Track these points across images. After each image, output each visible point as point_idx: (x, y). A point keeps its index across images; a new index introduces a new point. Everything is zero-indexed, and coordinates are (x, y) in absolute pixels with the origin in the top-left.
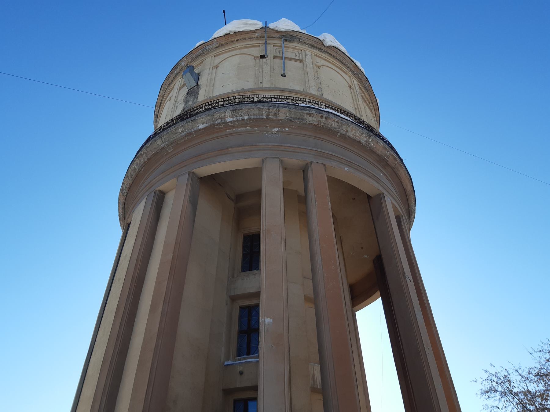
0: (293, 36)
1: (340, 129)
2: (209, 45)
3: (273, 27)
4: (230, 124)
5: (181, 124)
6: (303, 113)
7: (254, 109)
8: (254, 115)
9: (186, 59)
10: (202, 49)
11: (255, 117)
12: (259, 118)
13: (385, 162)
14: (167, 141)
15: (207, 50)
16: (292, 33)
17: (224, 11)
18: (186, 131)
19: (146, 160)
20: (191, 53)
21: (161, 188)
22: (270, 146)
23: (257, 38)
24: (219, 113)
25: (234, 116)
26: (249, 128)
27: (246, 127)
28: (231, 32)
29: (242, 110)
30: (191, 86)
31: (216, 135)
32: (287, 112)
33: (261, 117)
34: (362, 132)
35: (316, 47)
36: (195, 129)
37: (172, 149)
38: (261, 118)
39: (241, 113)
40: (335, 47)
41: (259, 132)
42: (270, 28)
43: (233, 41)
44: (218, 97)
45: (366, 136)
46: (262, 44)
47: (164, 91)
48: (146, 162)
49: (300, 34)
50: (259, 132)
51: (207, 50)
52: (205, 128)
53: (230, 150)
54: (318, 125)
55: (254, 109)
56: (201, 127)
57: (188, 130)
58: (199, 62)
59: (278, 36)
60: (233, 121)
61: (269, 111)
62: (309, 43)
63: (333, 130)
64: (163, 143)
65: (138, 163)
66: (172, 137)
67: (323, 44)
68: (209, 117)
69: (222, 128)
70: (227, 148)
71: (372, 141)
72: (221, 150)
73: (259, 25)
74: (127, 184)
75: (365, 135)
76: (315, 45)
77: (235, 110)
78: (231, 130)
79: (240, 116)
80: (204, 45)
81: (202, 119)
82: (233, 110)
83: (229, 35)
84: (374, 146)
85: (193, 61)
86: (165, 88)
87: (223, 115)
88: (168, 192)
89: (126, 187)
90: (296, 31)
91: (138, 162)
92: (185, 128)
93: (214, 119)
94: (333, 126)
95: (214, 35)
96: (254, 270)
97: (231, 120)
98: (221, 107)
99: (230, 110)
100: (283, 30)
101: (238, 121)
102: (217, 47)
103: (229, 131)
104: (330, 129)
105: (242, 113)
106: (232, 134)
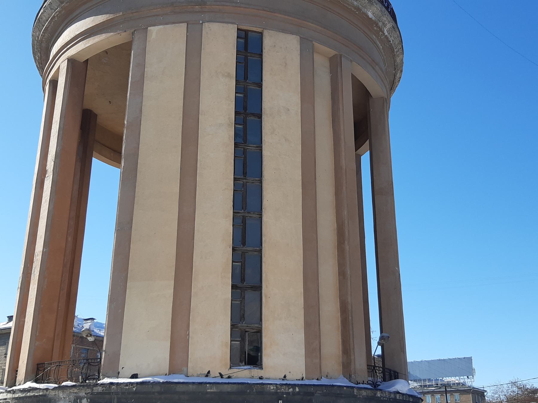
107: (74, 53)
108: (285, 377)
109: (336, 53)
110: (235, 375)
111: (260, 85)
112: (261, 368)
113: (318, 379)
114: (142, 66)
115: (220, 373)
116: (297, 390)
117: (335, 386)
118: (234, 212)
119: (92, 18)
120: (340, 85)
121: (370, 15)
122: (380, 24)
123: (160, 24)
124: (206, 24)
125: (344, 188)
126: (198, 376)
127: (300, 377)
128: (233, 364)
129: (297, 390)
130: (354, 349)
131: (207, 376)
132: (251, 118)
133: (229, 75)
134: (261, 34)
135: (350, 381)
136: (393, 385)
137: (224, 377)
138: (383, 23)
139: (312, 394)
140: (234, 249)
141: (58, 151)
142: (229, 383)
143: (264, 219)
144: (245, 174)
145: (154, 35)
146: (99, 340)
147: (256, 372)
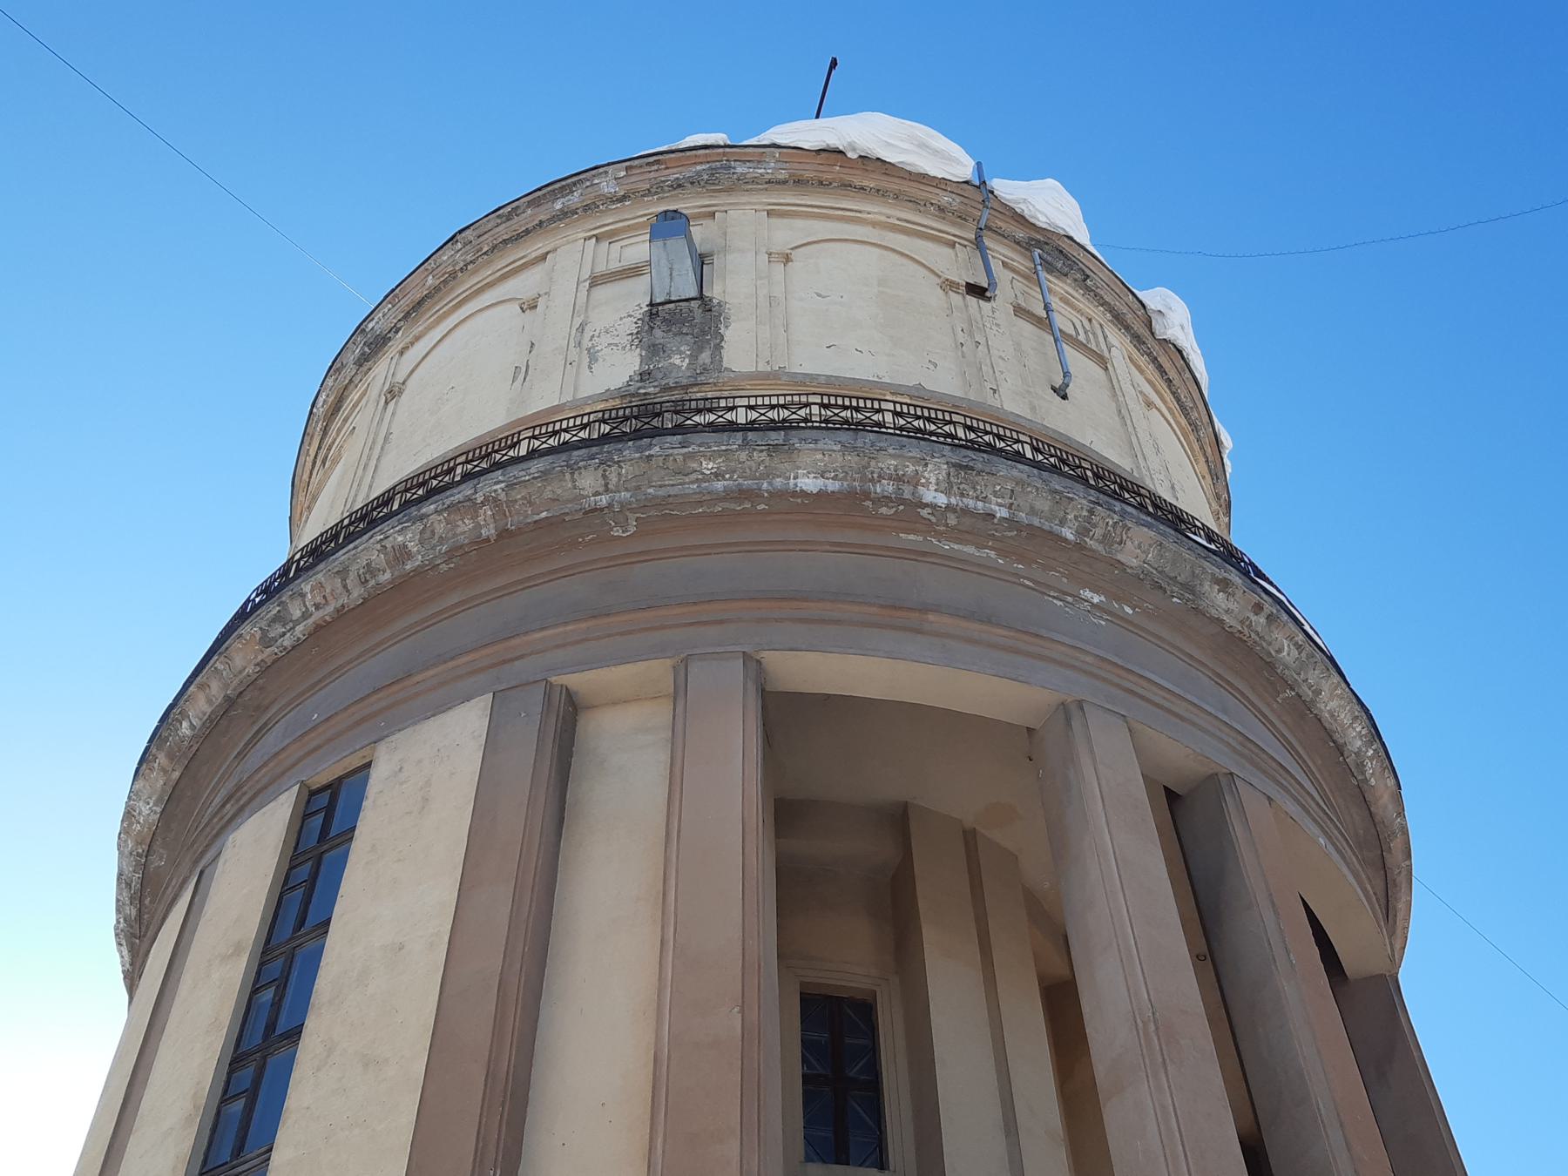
0: (1066, 257)
1: (1299, 674)
2: (745, 162)
3: (1008, 197)
4: (925, 512)
5: (719, 444)
6: (1204, 571)
7: (1037, 489)
8: (1033, 511)
9: (623, 173)
10: (714, 165)
11: (1036, 522)
12: (1050, 532)
13: (1380, 852)
14: (627, 490)
15: (735, 176)
16: (1065, 245)
17: (834, 63)
18: (731, 478)
19: (489, 531)
20: (657, 162)
21: (574, 680)
22: (1089, 659)
23: (941, 209)
24: (899, 456)
25: (955, 488)
26: (993, 554)
27: (980, 546)
28: (854, 150)
29: (992, 479)
30: (669, 294)
31: (853, 536)
32: (1150, 546)
33: (1056, 529)
34: (1356, 713)
35: (1127, 328)
36: (778, 482)
37: (633, 529)
38: (1057, 535)
39: (986, 486)
40: (1180, 352)
41: (1031, 584)
42: (996, 192)
43: (846, 186)
44: (828, 385)
45: (1363, 733)
46: (966, 243)
47: (469, 258)
48: (488, 540)
49: (1089, 260)
50: (1031, 584)
51: (735, 176)
52: (822, 495)
53: (931, 617)
54: (1237, 635)
55: (1037, 489)
56: (809, 484)
57: (746, 478)
58: (696, 211)
59: (1021, 234)
60: (949, 507)
61: (1088, 520)
62: (1112, 303)
63: (1279, 671)
64: (607, 490)
65: (433, 533)
66: (662, 479)
67: (1149, 324)
68: (852, 459)
69: (886, 517)
70: (924, 609)
71: (1371, 759)
72: (894, 607)
73: (961, 166)
74: (319, 599)
75: (1363, 728)
76: (1129, 317)
77: (967, 467)
78: (921, 538)
79: (977, 498)
80: (724, 154)
81: (819, 456)
82: (958, 466)
83: (840, 156)
84: (1372, 780)
85: (656, 193)
86: (482, 249)
87: (912, 468)
88: (588, 708)
89: (306, 615)
90: (1078, 240)
91: (440, 529)
92: (733, 464)
93: (873, 472)
94: (1281, 655)
95: (771, 130)
96: (854, 1165)
97: (942, 500)
98: (895, 434)
99: (947, 463)
100: (1042, 221)
101: (966, 511)
102: (779, 182)
103: (911, 537)
104: (1271, 666)
105: (990, 489)
106: (925, 554)
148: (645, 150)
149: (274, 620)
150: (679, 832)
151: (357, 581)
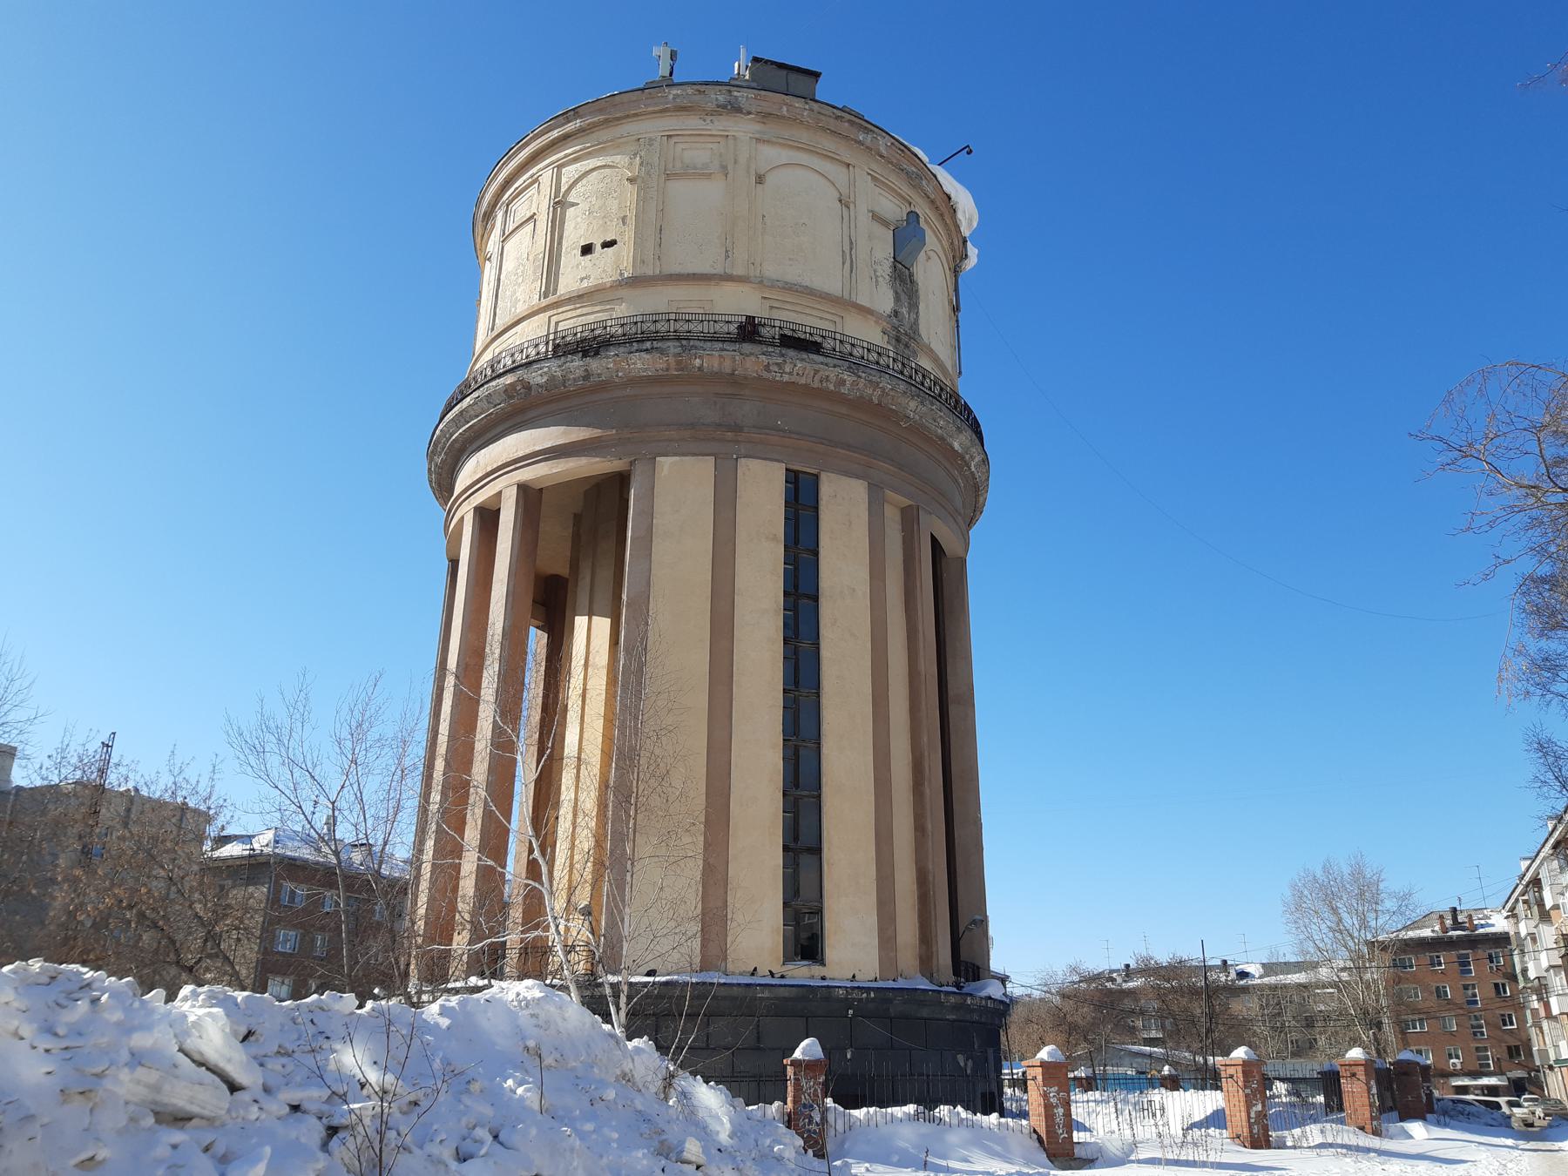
20: (902, 151)
23: (952, 243)
43: (942, 215)
72: (661, 230)
74: (800, 372)
91: (861, 385)
107: (530, 478)
108: (854, 976)
109: (910, 503)
110: (790, 973)
111: (816, 553)
112: (823, 964)
113: (894, 980)
114: (648, 513)
115: (770, 971)
116: (872, 995)
117: (919, 989)
118: (784, 740)
119: (562, 428)
120: (917, 550)
121: (956, 445)
122: (967, 457)
123: (675, 454)
124: (742, 461)
125: (923, 703)
126: (741, 974)
127: (873, 978)
128: (787, 959)
129: (872, 995)
130: (936, 936)
131: (753, 974)
132: (804, 601)
133: (775, 538)
134: (816, 477)
135: (931, 982)
136: (983, 988)
137: (776, 976)
138: (971, 456)
139: (1498, 1059)
140: (784, 795)
141: (506, 628)
142: (781, 985)
143: (825, 750)
144: (796, 683)
145: (666, 471)
146: (400, 890)
147: (817, 970)
148: (899, 136)
149: (777, 364)
150: (1507, 902)
151: (819, 378)
